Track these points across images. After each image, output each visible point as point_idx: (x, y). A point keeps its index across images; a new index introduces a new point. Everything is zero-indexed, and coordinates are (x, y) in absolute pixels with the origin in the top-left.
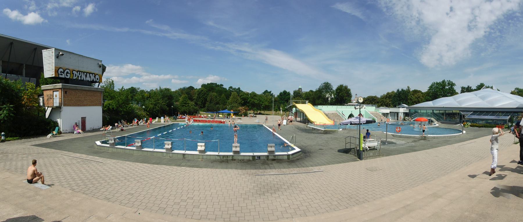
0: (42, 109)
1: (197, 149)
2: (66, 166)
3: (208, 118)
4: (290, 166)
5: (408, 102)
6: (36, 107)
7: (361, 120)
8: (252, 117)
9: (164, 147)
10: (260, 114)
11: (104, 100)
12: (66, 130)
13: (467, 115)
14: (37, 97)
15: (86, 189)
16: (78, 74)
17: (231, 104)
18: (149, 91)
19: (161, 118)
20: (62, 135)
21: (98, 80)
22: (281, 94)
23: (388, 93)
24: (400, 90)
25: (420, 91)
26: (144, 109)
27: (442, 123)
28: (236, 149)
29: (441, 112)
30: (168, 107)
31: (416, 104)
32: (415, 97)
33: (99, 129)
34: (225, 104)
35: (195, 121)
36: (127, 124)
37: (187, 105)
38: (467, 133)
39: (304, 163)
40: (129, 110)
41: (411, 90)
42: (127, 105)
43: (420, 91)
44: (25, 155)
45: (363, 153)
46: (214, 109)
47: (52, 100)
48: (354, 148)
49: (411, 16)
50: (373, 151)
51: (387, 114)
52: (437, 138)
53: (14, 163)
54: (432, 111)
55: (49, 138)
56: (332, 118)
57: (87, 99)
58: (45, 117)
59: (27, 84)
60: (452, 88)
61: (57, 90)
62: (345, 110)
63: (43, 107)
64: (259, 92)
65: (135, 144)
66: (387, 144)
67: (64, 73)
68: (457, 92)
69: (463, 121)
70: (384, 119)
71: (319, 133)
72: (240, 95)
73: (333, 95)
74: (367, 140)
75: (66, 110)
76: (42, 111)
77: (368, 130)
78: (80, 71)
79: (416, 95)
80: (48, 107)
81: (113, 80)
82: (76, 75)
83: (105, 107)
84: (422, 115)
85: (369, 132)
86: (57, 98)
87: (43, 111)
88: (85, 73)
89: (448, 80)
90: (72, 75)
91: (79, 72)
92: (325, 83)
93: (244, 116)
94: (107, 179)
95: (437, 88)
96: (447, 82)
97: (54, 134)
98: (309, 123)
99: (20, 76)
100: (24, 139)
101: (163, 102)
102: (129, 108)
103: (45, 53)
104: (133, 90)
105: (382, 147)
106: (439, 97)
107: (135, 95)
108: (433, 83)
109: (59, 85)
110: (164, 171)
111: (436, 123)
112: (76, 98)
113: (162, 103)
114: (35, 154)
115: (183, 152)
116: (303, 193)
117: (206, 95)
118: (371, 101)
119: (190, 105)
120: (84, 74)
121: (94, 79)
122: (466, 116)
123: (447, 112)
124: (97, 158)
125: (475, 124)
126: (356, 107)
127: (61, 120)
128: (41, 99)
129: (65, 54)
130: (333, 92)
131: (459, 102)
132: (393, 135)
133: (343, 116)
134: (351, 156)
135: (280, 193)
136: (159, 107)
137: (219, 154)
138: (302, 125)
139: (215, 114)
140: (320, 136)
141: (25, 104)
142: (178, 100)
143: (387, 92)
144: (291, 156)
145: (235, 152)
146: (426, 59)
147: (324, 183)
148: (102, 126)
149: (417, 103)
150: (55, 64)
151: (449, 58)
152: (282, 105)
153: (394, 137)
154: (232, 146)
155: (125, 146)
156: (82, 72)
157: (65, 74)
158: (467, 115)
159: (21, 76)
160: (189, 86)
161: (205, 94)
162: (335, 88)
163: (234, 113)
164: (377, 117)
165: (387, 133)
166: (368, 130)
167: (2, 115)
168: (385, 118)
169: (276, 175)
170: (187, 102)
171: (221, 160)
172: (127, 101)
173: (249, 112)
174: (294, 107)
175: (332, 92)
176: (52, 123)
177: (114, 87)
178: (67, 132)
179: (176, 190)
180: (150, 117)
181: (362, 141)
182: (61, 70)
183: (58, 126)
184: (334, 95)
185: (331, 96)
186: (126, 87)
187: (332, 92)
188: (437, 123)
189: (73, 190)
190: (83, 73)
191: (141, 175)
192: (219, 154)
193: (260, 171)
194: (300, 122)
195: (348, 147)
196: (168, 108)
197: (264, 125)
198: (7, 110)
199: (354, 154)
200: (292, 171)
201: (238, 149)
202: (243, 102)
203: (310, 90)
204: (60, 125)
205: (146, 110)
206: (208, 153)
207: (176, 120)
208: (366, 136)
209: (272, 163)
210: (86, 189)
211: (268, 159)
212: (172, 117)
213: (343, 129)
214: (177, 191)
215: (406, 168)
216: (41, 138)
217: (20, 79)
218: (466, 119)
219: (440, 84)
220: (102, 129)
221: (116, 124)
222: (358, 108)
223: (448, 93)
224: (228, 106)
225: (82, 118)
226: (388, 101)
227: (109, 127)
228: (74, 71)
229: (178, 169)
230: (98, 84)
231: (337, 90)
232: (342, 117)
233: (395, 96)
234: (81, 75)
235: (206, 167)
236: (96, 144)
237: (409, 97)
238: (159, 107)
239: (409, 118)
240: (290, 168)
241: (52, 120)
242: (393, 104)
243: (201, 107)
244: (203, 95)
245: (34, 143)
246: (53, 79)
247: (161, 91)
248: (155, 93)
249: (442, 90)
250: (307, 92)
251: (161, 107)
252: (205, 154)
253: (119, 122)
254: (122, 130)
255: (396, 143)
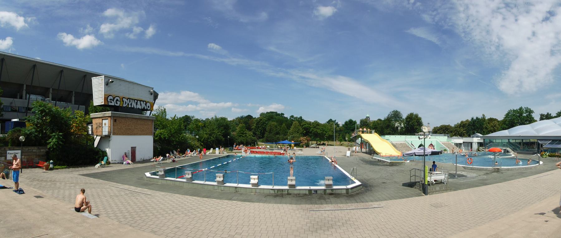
0: (91, 137)
1: (250, 182)
2: (114, 197)
3: (267, 149)
4: (348, 201)
5: (484, 131)
6: (84, 135)
7: (425, 151)
8: (315, 148)
9: (215, 180)
10: (324, 144)
11: (156, 129)
12: (115, 161)
13: (545, 144)
14: (86, 125)
15: (133, 222)
16: (128, 102)
17: (293, 134)
18: (204, 119)
19: (215, 149)
20: (111, 165)
21: (150, 108)
22: (346, 123)
23: (462, 122)
24: (475, 118)
25: (496, 119)
26: (197, 138)
27: (518, 153)
28: (291, 182)
29: (517, 141)
30: (224, 137)
31: (492, 133)
32: (491, 125)
33: (149, 159)
34: (285, 134)
35: (252, 152)
36: (179, 155)
37: (244, 135)
38: (544, 164)
39: (363, 198)
40: (182, 140)
41: (486, 118)
42: (179, 135)
43: (495, 120)
44: (72, 185)
45: (429, 187)
46: (273, 140)
47: (100, 129)
48: (419, 182)
49: (491, 41)
50: (440, 185)
51: (460, 144)
52: (511, 169)
53: (62, 191)
54: (507, 141)
55: (97, 168)
56: (400, 149)
57: (137, 127)
58: (94, 145)
59: (76, 111)
60: (530, 115)
61: (107, 118)
62: (413, 140)
63: (92, 136)
64: (323, 121)
65: (185, 176)
66: (456, 177)
67: (113, 101)
68: (535, 119)
69: (541, 151)
70: (457, 150)
71: (384, 165)
72: (302, 124)
73: (402, 124)
74: (433, 173)
75: (115, 139)
76: (90, 140)
77: (434, 162)
78: (130, 99)
79: (491, 124)
80: (97, 136)
81: (165, 108)
82: (126, 102)
83: (157, 137)
84: (497, 145)
85: (435, 164)
86: (106, 126)
87: (92, 140)
88: (136, 101)
89: (526, 107)
90: (122, 103)
91: (129, 100)
92: (394, 111)
93: (306, 147)
94: (154, 212)
95: (514, 115)
96: (525, 109)
97: (102, 164)
98: (375, 154)
99: (69, 103)
100: (72, 168)
101: (218, 132)
102: (182, 137)
103: (95, 80)
104: (187, 119)
105: (450, 180)
106: (516, 125)
107: (189, 124)
108: (509, 110)
109: (109, 113)
110: (213, 205)
111: (512, 153)
112: (125, 126)
113: (218, 133)
114: (82, 183)
115: (235, 185)
116: (358, 231)
117: (265, 125)
118: (444, 130)
119: (247, 135)
120: (134, 101)
121: (145, 106)
122: (544, 145)
123: (524, 141)
124: (146, 191)
125: (553, 154)
126: (420, 136)
127: (110, 149)
128: (90, 127)
129: (115, 81)
130: (402, 121)
131: (536, 130)
132: (464, 167)
133: (412, 146)
134: (416, 191)
135: (334, 230)
136: (214, 137)
137: (273, 187)
138: (367, 157)
139: (274, 145)
140: (385, 168)
141: (74, 132)
142: (235, 130)
143: (461, 121)
144: (350, 190)
145: (292, 186)
146: (505, 85)
147: (383, 220)
148: (152, 157)
149: (492, 132)
150: (105, 91)
151: (530, 84)
152: (347, 135)
153: (465, 169)
154: (287, 179)
155: (175, 177)
156: (132, 99)
157: (115, 102)
158: (545, 144)
159: (70, 103)
160: (248, 115)
161: (264, 123)
162: (404, 116)
163: (295, 144)
164: (449, 148)
165: (457, 165)
166: (434, 162)
167: (51, 143)
168: (458, 148)
169: (332, 211)
170: (245, 132)
171: (275, 194)
172: (179, 131)
173: (310, 142)
174: (359, 137)
175: (401, 121)
176: (101, 153)
177: (165, 115)
178: (116, 162)
179: (225, 225)
180: (204, 148)
181: (427, 174)
182: (111, 97)
183: (106, 156)
184: (404, 124)
185: (401, 125)
186: (180, 115)
187: (401, 121)
188: (513, 154)
189: (120, 222)
190: (133, 101)
191: (189, 209)
192: (273, 187)
193: (316, 206)
194: (366, 153)
195: (413, 181)
196: (224, 139)
197: (325, 157)
198: (56, 138)
199: (419, 188)
200: (349, 207)
201: (294, 183)
202: (305, 131)
203: (378, 119)
204: (108, 155)
205: (200, 141)
206: (262, 187)
207: (232, 151)
208: (432, 169)
209: (328, 197)
210: (133, 222)
211: (325, 194)
212: (228, 149)
213: (411, 161)
214: (225, 226)
215: (474, 204)
216: (89, 168)
217: (70, 107)
218: (545, 149)
219: (517, 111)
220: (153, 160)
221: (167, 155)
222: (422, 139)
223: (526, 121)
224: (289, 136)
225: (132, 147)
226: (462, 130)
227: (160, 158)
228: (124, 99)
229: (228, 203)
230: (149, 112)
231: (406, 119)
232: (411, 148)
233: (469, 125)
234: (131, 103)
235: (259, 201)
236: (146, 175)
237: (484, 126)
238: (214, 137)
239: (483, 149)
240: (347, 203)
241: (100, 149)
242: (467, 133)
243: (260, 138)
244: (262, 125)
245: (81, 173)
246: (102, 107)
247: (217, 120)
248: (210, 122)
249: (519, 118)
250: (374, 121)
251: (216, 137)
252: (258, 188)
253: (171, 153)
254: (174, 161)
255: (466, 176)
